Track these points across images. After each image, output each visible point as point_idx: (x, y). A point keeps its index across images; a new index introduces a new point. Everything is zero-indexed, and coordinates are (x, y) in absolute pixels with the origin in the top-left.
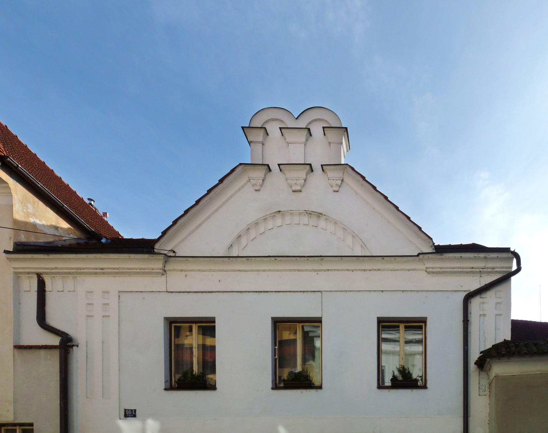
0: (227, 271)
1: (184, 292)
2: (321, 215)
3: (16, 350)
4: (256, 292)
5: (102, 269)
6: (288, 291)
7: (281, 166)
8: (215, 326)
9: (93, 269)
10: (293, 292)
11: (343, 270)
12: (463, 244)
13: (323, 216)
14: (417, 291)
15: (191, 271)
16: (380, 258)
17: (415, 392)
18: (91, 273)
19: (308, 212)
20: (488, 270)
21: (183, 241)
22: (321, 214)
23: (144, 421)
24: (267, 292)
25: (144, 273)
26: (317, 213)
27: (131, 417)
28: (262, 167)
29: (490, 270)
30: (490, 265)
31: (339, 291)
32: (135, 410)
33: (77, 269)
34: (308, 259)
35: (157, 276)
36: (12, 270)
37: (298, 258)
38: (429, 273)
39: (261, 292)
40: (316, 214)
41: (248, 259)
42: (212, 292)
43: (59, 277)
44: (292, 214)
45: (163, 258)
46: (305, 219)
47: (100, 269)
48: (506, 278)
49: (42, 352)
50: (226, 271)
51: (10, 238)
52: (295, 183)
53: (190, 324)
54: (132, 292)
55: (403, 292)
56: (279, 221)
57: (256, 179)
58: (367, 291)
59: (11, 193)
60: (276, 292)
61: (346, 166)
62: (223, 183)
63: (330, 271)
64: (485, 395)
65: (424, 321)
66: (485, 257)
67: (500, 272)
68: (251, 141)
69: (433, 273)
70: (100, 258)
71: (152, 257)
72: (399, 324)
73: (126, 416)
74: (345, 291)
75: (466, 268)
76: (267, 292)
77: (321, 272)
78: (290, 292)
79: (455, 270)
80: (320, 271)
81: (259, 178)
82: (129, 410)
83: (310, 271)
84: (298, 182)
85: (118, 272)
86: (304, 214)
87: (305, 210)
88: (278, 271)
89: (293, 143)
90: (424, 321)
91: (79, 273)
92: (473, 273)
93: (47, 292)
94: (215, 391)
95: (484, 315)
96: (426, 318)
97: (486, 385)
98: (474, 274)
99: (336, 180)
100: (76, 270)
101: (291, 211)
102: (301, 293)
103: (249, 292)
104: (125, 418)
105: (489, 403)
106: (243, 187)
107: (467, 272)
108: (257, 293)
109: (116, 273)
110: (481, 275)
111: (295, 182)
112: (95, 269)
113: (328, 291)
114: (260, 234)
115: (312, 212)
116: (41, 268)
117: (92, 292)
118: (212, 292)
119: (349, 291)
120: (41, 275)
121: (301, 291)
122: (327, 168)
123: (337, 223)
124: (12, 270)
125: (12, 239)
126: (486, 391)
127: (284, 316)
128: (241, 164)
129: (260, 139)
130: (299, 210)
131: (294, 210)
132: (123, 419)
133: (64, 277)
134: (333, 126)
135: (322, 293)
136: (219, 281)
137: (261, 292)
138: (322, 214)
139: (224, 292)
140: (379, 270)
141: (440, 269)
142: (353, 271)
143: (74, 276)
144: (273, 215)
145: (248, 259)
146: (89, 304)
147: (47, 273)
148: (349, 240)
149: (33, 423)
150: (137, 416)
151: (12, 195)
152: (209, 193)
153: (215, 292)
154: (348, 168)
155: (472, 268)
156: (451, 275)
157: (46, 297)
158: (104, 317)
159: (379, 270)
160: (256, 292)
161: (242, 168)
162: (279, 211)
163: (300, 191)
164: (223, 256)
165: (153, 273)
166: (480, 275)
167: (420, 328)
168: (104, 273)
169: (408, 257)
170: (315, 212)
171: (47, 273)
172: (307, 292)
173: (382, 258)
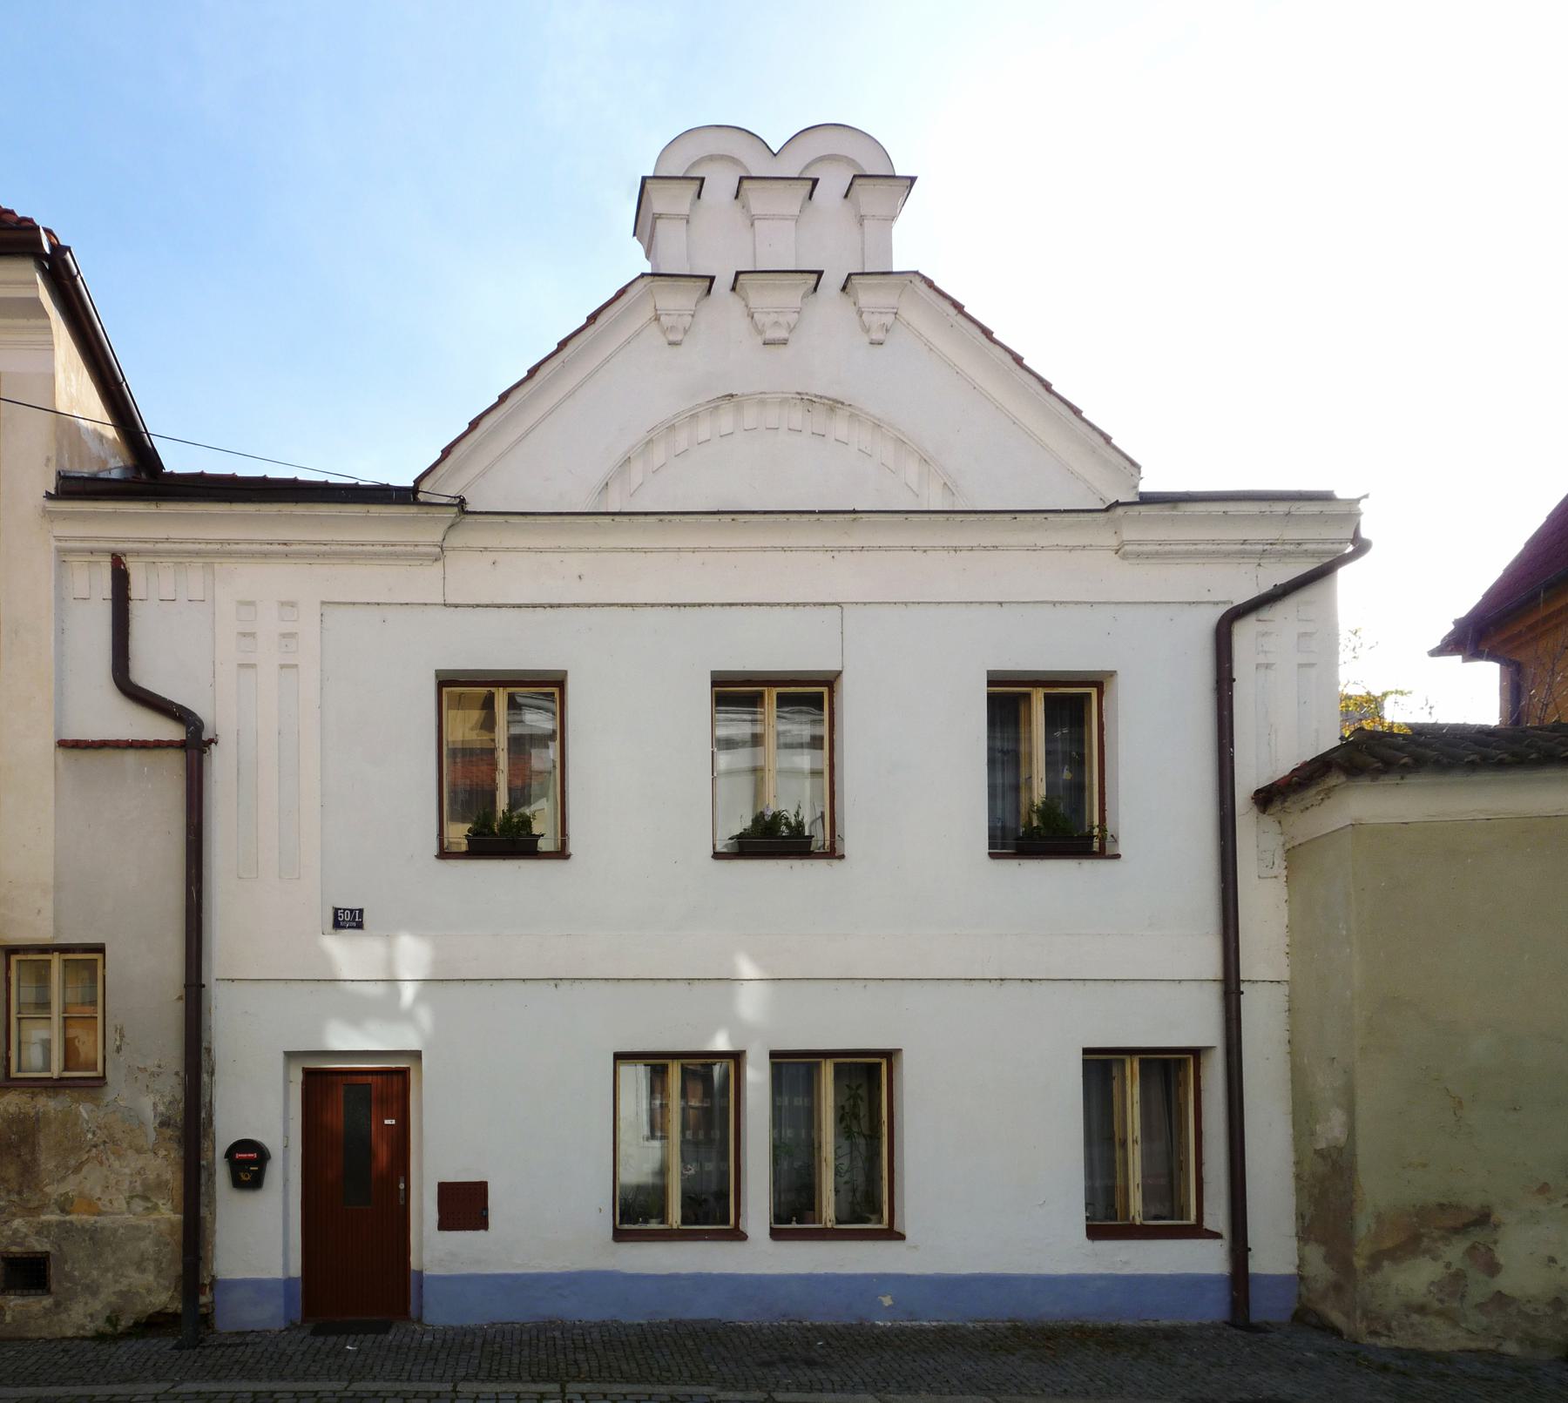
0: (598, 550)
1: (487, 606)
2: (840, 405)
3: (60, 751)
4: (672, 605)
5: (285, 544)
6: (755, 604)
7: (813, 278)
8: (988, 686)
9: (262, 543)
10: (768, 604)
11: (901, 549)
12: (269, 476)
13: (845, 408)
14: (1092, 604)
15: (508, 550)
16: (1008, 517)
17: (1088, 866)
18: (252, 555)
19: (806, 397)
20: (1287, 547)
21: (483, 474)
22: (838, 402)
23: (389, 938)
24: (700, 605)
25: (396, 556)
26: (829, 399)
27: (349, 927)
28: (695, 282)
29: (1292, 547)
30: (1293, 534)
31: (889, 603)
32: (361, 911)
33: (222, 542)
34: (819, 520)
35: (421, 562)
36: (54, 544)
37: (793, 517)
38: (1125, 557)
39: (685, 605)
40: (826, 401)
41: (661, 520)
42: (559, 606)
43: (170, 564)
44: (762, 403)
45: (454, 515)
46: (796, 416)
47: (279, 544)
48: (1323, 573)
49: (131, 757)
50: (595, 552)
51: (48, 459)
52: (776, 322)
53: (489, 689)
54: (354, 604)
55: (1054, 605)
56: (726, 421)
57: (674, 315)
58: (1149, 603)
59: (53, 344)
60: (722, 605)
61: (911, 277)
62: (597, 322)
63: (866, 552)
64: (1276, 877)
65: (830, 681)
66: (1288, 514)
67: (1313, 554)
68: (660, 214)
69: (1138, 555)
70: (291, 514)
71: (427, 513)
72: (1031, 689)
73: (337, 925)
74: (902, 603)
75: (1229, 542)
76: (700, 605)
77: (842, 553)
78: (760, 605)
79: (1198, 547)
80: (645, 552)
81: (681, 313)
82: (345, 910)
83: (815, 550)
84: (781, 319)
85: (325, 552)
86: (795, 401)
87: (799, 391)
88: (729, 550)
89: (767, 219)
90: (830, 681)
91: (226, 552)
92: (1243, 554)
93: (134, 601)
94: (566, 861)
95: (1268, 666)
96: (565, 673)
97: (1274, 851)
98: (1243, 557)
99: (881, 313)
100: (219, 546)
101: (763, 396)
102: (789, 607)
103: (653, 605)
104: (333, 931)
105: (1286, 898)
106: (638, 334)
107: (1227, 555)
108: (674, 608)
109: (318, 555)
110: (1262, 561)
111: (773, 317)
112: (268, 544)
113: (899, 603)
114: (676, 456)
115: (816, 396)
116: (127, 540)
117: (252, 603)
118: (559, 606)
119: (913, 603)
120: (123, 558)
121: (788, 604)
122: (861, 281)
123: (882, 424)
124: (54, 544)
125: (54, 462)
126: (1276, 865)
127: (744, 667)
128: (916, 273)
129: (684, 207)
130: (783, 393)
131: (769, 393)
132: (330, 934)
133: (181, 563)
134: (754, 175)
135: (842, 608)
136: (580, 577)
137: (685, 605)
138: (843, 403)
139: (590, 606)
140: (996, 548)
141: (1160, 544)
142: (925, 551)
143: (208, 560)
144: (713, 405)
145: (661, 520)
146: (244, 635)
147: (138, 553)
148: (912, 470)
149: (104, 944)
150: (365, 926)
151: (53, 350)
152: (562, 349)
153: (568, 606)
154: (917, 280)
155: (1244, 542)
156: (1183, 561)
157: (130, 616)
158: (281, 668)
159: (996, 548)
160: (672, 605)
161: (645, 286)
162: (732, 396)
163: (784, 342)
164: (586, 511)
165: (418, 554)
166: (1257, 561)
167: (815, 702)
168: (92, 553)
169: (1081, 515)
170: (826, 398)
171: (138, 553)
172: (805, 604)
173: (1013, 516)
